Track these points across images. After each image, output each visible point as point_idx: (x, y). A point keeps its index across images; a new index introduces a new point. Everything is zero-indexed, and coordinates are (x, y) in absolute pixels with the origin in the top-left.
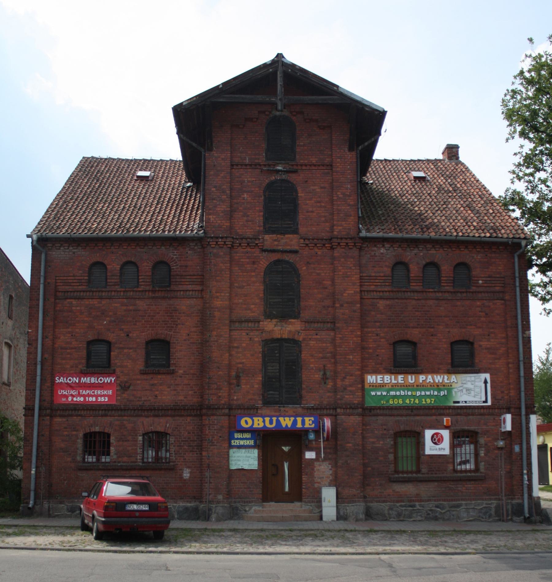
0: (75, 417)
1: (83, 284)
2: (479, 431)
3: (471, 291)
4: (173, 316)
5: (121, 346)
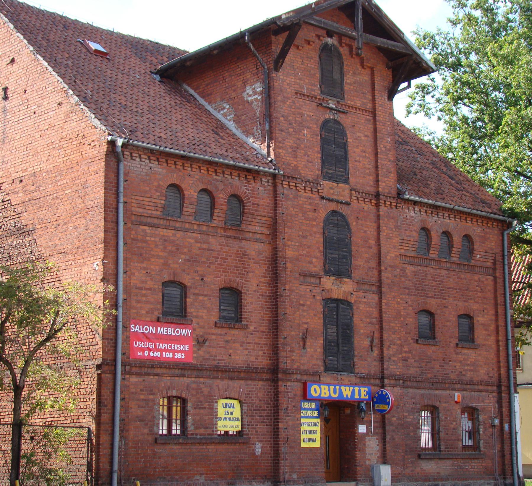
0: (152, 377)
1: (158, 209)
2: (479, 408)
3: (471, 264)
4: (244, 261)
5: (197, 291)
